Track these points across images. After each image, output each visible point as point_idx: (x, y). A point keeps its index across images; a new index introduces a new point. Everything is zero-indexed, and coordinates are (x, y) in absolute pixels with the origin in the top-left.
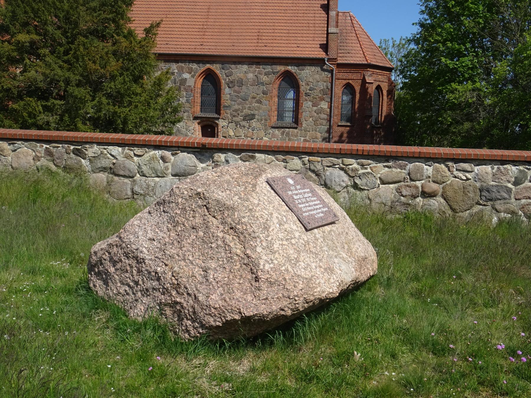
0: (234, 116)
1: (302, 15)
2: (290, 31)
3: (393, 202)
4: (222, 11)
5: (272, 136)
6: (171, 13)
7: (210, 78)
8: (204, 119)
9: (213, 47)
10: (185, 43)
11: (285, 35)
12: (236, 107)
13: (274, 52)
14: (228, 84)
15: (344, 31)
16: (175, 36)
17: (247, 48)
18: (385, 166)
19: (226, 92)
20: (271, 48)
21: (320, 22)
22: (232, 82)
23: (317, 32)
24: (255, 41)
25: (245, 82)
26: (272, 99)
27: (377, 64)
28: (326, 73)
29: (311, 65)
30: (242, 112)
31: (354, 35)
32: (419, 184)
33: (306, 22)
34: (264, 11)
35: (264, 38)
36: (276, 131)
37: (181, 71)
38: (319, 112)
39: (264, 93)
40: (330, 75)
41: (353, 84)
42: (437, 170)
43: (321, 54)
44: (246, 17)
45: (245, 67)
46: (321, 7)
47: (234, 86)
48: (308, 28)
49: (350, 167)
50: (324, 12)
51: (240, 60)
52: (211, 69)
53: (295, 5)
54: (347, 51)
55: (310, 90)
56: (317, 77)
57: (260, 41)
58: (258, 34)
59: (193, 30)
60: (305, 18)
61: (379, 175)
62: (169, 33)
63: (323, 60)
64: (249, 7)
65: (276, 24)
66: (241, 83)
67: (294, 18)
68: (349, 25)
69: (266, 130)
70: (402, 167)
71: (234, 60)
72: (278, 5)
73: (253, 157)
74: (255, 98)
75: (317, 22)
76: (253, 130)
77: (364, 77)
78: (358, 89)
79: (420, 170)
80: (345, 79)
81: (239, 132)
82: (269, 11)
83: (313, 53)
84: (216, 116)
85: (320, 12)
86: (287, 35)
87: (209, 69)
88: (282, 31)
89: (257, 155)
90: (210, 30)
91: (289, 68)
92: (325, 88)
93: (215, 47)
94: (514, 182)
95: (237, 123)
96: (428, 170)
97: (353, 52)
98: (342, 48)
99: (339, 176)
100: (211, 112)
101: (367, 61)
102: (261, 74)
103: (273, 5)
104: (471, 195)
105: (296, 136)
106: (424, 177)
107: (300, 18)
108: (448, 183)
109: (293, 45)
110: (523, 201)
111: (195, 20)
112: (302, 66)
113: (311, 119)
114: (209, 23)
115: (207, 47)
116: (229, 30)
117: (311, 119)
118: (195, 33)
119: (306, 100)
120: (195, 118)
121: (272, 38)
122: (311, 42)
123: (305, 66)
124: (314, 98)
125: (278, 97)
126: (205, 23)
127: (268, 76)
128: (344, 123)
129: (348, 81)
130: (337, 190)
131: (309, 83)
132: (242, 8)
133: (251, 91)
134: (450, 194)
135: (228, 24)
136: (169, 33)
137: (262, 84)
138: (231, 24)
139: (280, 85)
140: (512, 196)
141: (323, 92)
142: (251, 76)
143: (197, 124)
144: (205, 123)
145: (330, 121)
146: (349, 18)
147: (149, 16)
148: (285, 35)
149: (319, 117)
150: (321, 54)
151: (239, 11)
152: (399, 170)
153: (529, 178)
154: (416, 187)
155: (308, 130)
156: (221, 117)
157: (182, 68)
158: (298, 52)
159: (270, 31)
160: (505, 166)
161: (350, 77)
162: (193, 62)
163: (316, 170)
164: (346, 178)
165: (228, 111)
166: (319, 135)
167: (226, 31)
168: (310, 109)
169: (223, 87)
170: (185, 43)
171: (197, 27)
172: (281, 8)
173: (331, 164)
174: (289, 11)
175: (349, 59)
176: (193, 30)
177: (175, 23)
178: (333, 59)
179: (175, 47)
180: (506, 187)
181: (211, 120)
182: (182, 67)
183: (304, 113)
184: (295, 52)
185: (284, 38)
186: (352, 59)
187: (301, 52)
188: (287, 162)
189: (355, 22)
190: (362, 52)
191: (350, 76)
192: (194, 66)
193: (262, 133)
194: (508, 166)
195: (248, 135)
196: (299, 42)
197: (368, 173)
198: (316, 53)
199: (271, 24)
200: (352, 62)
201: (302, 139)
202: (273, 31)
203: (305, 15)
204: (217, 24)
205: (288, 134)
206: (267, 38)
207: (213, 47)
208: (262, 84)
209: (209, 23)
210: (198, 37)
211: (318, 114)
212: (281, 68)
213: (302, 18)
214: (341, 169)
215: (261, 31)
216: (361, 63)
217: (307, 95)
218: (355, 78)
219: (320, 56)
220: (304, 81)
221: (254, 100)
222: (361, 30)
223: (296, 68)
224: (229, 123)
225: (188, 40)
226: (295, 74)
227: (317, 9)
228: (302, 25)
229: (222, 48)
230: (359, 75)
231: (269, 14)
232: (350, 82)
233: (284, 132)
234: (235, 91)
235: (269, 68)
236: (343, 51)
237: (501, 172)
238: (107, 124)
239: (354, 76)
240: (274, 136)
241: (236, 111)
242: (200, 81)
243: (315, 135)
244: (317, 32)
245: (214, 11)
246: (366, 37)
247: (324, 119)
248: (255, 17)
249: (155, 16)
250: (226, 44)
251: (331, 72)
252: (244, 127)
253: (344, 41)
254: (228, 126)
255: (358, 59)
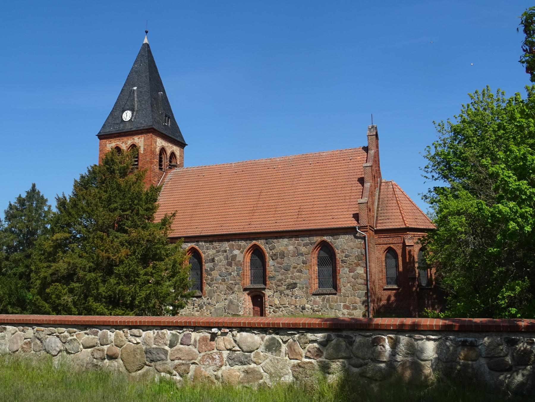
0: (279, 286)
1: (340, 189)
2: (328, 205)
3: (88, 364)
4: (271, 193)
5: (313, 303)
6: (230, 199)
7: (257, 252)
8: (253, 290)
9: (258, 226)
10: (236, 224)
11: (322, 209)
12: (280, 277)
13: (310, 225)
14: (272, 257)
15: (386, 199)
16: (229, 219)
17: (287, 224)
18: (86, 333)
19: (270, 263)
20: (308, 222)
21: (355, 194)
22: (275, 255)
23: (352, 203)
24: (296, 217)
25: (287, 253)
26: (311, 268)
27: (418, 227)
28: (359, 240)
29: (345, 234)
30: (285, 282)
31: (395, 202)
32: (105, 347)
33: (343, 195)
34: (307, 189)
35: (303, 213)
36: (317, 298)
37: (232, 248)
38: (356, 277)
39: (304, 262)
40: (363, 242)
41: (394, 248)
42: (117, 336)
43: (354, 223)
44: (291, 197)
45: (285, 241)
46: (358, 181)
47: (277, 258)
48: (344, 201)
49: (62, 334)
50: (360, 185)
51: (259, 236)
52: (257, 244)
53: (334, 181)
54: (387, 218)
55: (345, 257)
56: (351, 244)
57: (300, 216)
58: (299, 210)
59: (245, 212)
60: (343, 192)
61: (81, 341)
62: (225, 216)
63: (354, 228)
64: (294, 188)
65: (316, 200)
66: (283, 255)
67: (332, 193)
68: (391, 193)
69: (307, 297)
70: (96, 334)
71: (276, 235)
72: (320, 183)
73: (5, 329)
74: (296, 268)
75: (353, 194)
76: (296, 298)
77: (404, 241)
78: (399, 252)
79: (105, 336)
80: (386, 244)
81: (284, 300)
82: (311, 189)
83: (346, 222)
84: (263, 286)
85: (356, 185)
86: (324, 208)
87: (255, 245)
88: (320, 206)
89: (7, 327)
90: (259, 211)
91: (325, 238)
92: (360, 254)
93: (260, 226)
94: (170, 345)
95: (281, 292)
96: (111, 335)
97: (393, 217)
98: (382, 215)
99: (55, 343)
100: (259, 283)
101: (405, 225)
102: (300, 246)
103: (315, 183)
104: (138, 357)
105: (336, 302)
106: (109, 342)
107: (338, 192)
108: (124, 346)
109: (328, 217)
110: (176, 362)
111: (248, 203)
112: (336, 235)
113: (349, 285)
114: (258, 205)
115: (253, 226)
116: (275, 210)
117: (349, 285)
118: (246, 215)
119: (343, 267)
120: (245, 290)
121: (310, 212)
122: (345, 213)
123: (339, 235)
124: (350, 264)
125: (318, 265)
126: (256, 205)
127: (306, 248)
128: (389, 287)
129: (389, 245)
130: (54, 354)
131: (344, 251)
132: (288, 189)
133: (293, 261)
134: (124, 356)
135: (274, 204)
136: (225, 216)
137: (302, 254)
138: (277, 204)
139: (319, 254)
140: (168, 358)
141: (358, 258)
142: (291, 248)
143: (247, 295)
144: (254, 294)
145: (367, 285)
146: (391, 187)
147: (211, 204)
148: (322, 209)
149: (356, 282)
150: (354, 223)
151: (285, 192)
152: (93, 336)
153: (180, 341)
154: (103, 350)
155: (347, 295)
156: (268, 286)
157: (233, 245)
158: (332, 223)
159: (310, 207)
160: (162, 331)
161: (391, 242)
162: (242, 239)
163: (40, 337)
164: (60, 344)
165: (273, 282)
166: (358, 300)
167: (272, 210)
168: (347, 275)
169: (267, 260)
170: (236, 224)
171: (248, 209)
172: (322, 185)
173: (50, 333)
174: (328, 188)
175: (388, 224)
176: (245, 212)
177: (231, 207)
178: (365, 226)
179: (228, 228)
180: (164, 349)
181: (258, 290)
182: (233, 245)
183: (342, 280)
184: (329, 224)
185: (321, 212)
186: (391, 224)
187: (335, 223)
188: (25, 332)
189: (397, 190)
190: (401, 217)
191: (391, 240)
192: (243, 243)
193: (304, 300)
194: (165, 331)
195: (292, 303)
196: (334, 214)
197: (75, 339)
198: (349, 222)
199: (312, 200)
200: (391, 227)
201: (342, 304)
202: (312, 206)
203: (343, 189)
204: (265, 205)
205: (328, 300)
206: (306, 213)
207: (258, 226)
208: (302, 254)
209: (258, 205)
210: (247, 218)
211: (355, 279)
212: (317, 239)
213: (340, 192)
214: (58, 336)
215: (302, 207)
216: (399, 227)
217: (343, 261)
218: (395, 242)
219: (352, 225)
220: (339, 249)
221: (295, 270)
222: (403, 196)
223: (331, 237)
224: (275, 292)
225: (239, 221)
226: (330, 244)
227: (354, 182)
228: (339, 198)
229: (266, 225)
230: (399, 239)
231: (311, 192)
232: (392, 246)
233: (324, 298)
234: (278, 263)
235: (307, 240)
236: (383, 218)
237: (159, 336)
238: (115, 302)
239: (395, 240)
240: (315, 302)
241: (280, 281)
242: (248, 257)
243: (354, 300)
244: (352, 203)
245: (264, 194)
246: (409, 202)
247: (361, 284)
248: (298, 196)
249: (216, 203)
250: (271, 222)
251: (364, 238)
252: (288, 295)
253: (385, 208)
254: (273, 296)
255: (397, 224)
